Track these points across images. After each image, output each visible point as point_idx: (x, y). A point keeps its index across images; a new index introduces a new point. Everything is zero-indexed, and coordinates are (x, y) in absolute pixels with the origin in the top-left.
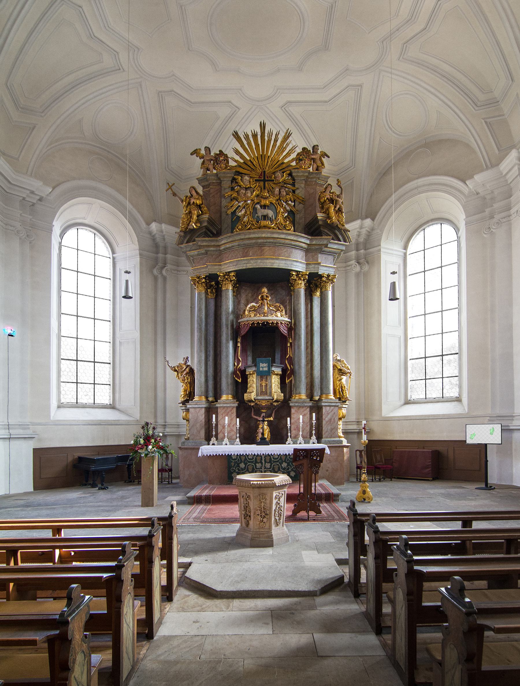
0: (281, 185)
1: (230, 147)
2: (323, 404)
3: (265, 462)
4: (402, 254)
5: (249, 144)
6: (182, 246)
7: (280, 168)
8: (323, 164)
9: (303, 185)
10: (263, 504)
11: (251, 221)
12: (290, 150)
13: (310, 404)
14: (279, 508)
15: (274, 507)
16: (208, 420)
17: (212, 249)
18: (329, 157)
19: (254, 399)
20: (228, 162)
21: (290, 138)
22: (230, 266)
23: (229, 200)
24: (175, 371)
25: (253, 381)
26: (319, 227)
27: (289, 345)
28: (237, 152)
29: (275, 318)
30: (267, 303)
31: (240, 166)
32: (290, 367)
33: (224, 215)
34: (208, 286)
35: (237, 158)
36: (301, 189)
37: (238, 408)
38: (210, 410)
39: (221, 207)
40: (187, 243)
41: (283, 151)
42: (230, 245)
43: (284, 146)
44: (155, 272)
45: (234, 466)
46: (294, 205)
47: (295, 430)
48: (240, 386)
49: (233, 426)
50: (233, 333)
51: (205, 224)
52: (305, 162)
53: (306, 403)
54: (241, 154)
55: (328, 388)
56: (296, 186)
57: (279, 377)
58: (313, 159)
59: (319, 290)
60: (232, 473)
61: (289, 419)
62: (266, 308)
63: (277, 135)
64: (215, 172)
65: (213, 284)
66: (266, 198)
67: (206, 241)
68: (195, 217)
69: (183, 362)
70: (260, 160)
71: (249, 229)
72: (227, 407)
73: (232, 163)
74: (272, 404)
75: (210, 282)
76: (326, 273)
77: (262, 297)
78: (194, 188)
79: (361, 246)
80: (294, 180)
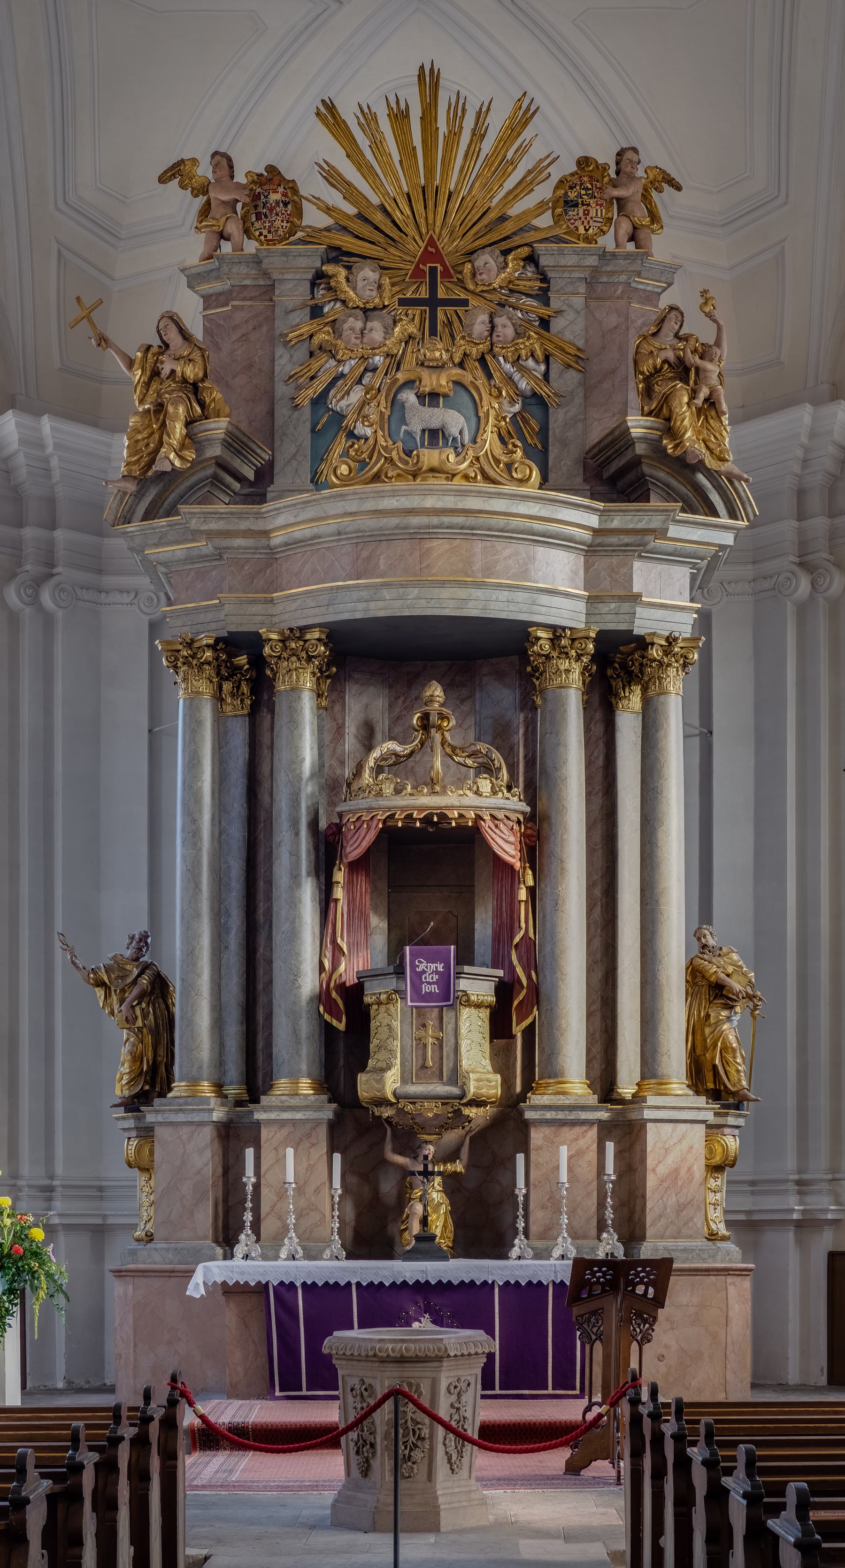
0: (496, 297)
1: (305, 153)
2: (648, 1114)
5: (377, 145)
7: (495, 236)
8: (654, 217)
9: (578, 301)
11: (385, 448)
12: (530, 172)
13: (604, 1115)
16: (230, 1171)
17: (239, 542)
18: (679, 188)
19: (394, 1094)
20: (299, 212)
23: (301, 353)
25: (394, 1027)
27: (523, 894)
28: (332, 177)
29: (470, 799)
30: (443, 742)
32: (529, 977)
33: (282, 412)
34: (225, 672)
36: (570, 315)
37: (334, 1127)
38: (235, 1136)
39: (272, 377)
40: (145, 518)
41: (506, 175)
43: (509, 156)
46: (546, 376)
47: (544, 1207)
48: (347, 1028)
49: (317, 1191)
50: (316, 848)
51: (215, 451)
52: (586, 213)
54: (349, 184)
56: (555, 303)
57: (485, 1014)
58: (621, 203)
59: (637, 690)
63: (481, 115)
64: (251, 247)
65: (244, 669)
66: (440, 367)
67: (220, 516)
68: (178, 429)
69: (128, 953)
70: (419, 207)
71: (376, 478)
72: (294, 1122)
73: (314, 218)
75: (231, 655)
77: (425, 717)
78: (174, 319)
80: (545, 279)
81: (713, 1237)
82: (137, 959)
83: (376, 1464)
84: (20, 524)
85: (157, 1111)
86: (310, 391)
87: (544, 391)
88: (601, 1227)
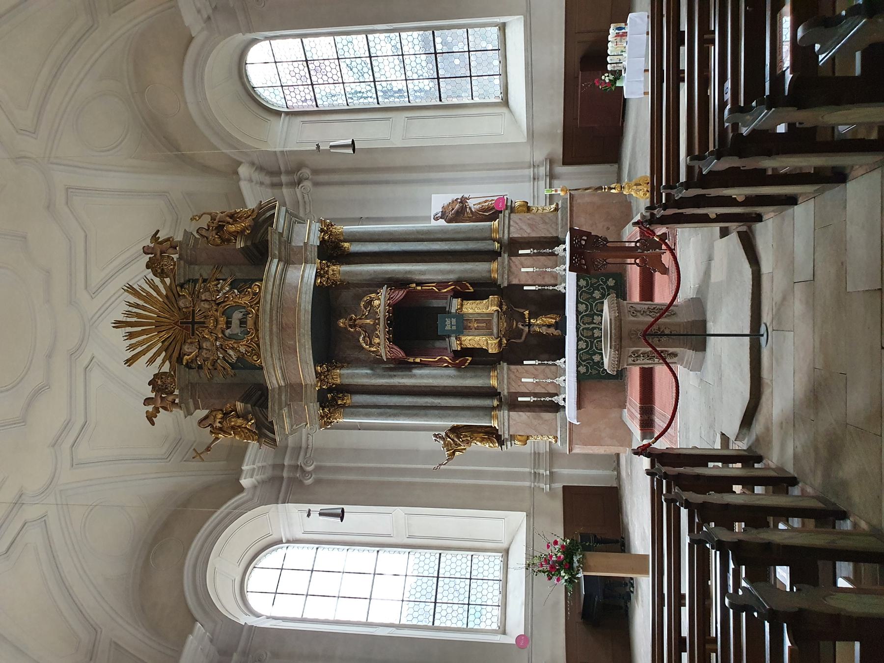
4: (287, 118)
6: (278, 440)
7: (173, 300)
8: (168, 240)
9: (197, 267)
13: (506, 255)
16: (527, 407)
18: (158, 231)
21: (135, 286)
22: (306, 371)
23: (215, 373)
24: (454, 453)
25: (471, 341)
26: (249, 244)
27: (419, 288)
28: (151, 361)
29: (382, 308)
31: (171, 357)
35: (159, 360)
38: (513, 405)
44: (309, 482)
46: (224, 280)
48: (478, 359)
50: (401, 368)
53: (503, 263)
55: (482, 230)
56: (197, 276)
57: (465, 302)
58: (162, 252)
61: (525, 288)
62: (368, 321)
64: (176, 392)
65: (332, 399)
66: (217, 321)
68: (240, 421)
70: (163, 328)
71: (258, 345)
72: (509, 378)
73: (166, 368)
74: (504, 313)
79: (275, 180)
81: (556, 209)
83: (671, 350)
87: (229, 281)
88: (553, 254)
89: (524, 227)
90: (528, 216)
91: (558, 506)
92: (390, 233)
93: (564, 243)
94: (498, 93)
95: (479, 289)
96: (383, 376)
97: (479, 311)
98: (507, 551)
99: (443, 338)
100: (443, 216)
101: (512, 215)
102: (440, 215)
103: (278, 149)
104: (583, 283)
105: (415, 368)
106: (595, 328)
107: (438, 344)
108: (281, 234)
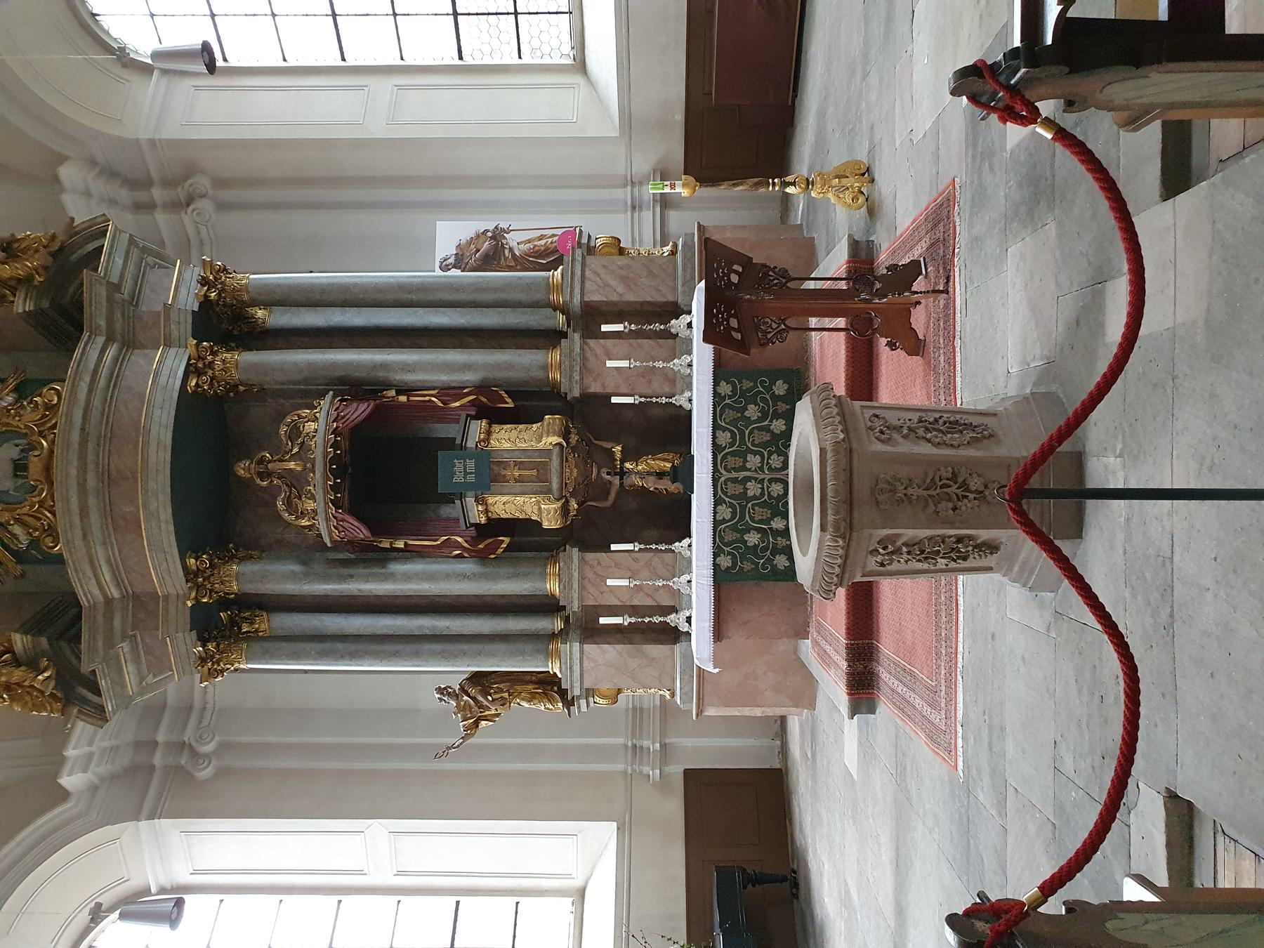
2: (577, 300)
3: (744, 468)
4: (165, 80)
10: (914, 491)
13: (577, 336)
14: (927, 430)
15: (925, 449)
19: (558, 500)
22: (164, 568)
24: (476, 724)
25: (506, 505)
27: (403, 398)
29: (319, 438)
37: (585, 547)
38: (591, 631)
40: (100, 695)
42: (105, 569)
44: (205, 773)
45: (753, 563)
48: (521, 540)
51: (44, 641)
53: (572, 351)
55: (530, 286)
57: (496, 427)
59: (251, 310)
60: (774, 567)
61: (614, 400)
62: (292, 465)
65: (225, 625)
68: (18, 674)
72: (582, 578)
74: (574, 449)
76: (196, 289)
79: (141, 196)
81: (673, 253)
82: (457, 696)
83: (984, 535)
84: (152, 768)
85: (572, 687)
86: (10, 565)
87: (12, 383)
89: (613, 283)
90: (621, 261)
91: (674, 808)
92: (344, 288)
93: (689, 312)
94: (567, 48)
95: (526, 403)
96: (326, 578)
97: (524, 445)
98: (582, 893)
99: (449, 499)
100: (460, 262)
101: (589, 259)
102: (452, 260)
103: (144, 134)
104: (725, 388)
105: (395, 559)
106: (748, 479)
107: (447, 511)
108: (117, 287)
